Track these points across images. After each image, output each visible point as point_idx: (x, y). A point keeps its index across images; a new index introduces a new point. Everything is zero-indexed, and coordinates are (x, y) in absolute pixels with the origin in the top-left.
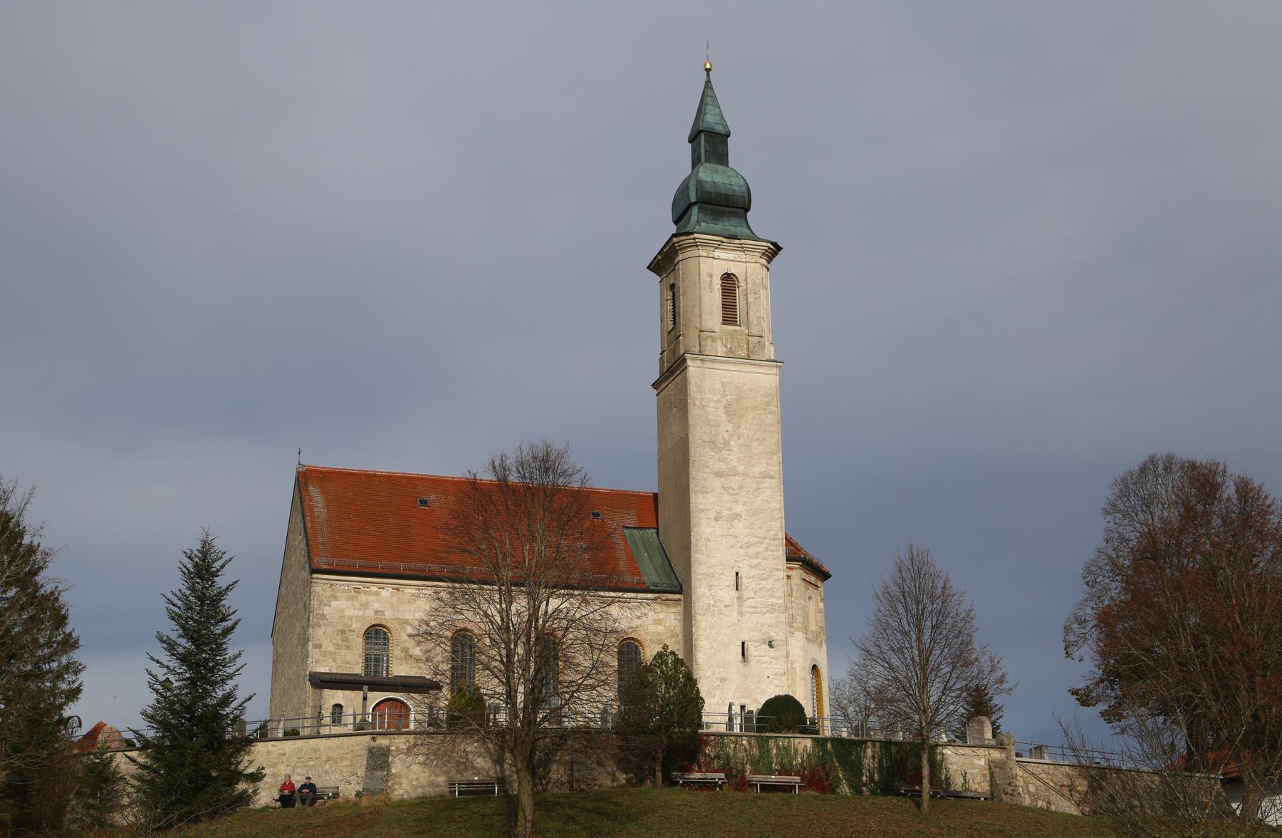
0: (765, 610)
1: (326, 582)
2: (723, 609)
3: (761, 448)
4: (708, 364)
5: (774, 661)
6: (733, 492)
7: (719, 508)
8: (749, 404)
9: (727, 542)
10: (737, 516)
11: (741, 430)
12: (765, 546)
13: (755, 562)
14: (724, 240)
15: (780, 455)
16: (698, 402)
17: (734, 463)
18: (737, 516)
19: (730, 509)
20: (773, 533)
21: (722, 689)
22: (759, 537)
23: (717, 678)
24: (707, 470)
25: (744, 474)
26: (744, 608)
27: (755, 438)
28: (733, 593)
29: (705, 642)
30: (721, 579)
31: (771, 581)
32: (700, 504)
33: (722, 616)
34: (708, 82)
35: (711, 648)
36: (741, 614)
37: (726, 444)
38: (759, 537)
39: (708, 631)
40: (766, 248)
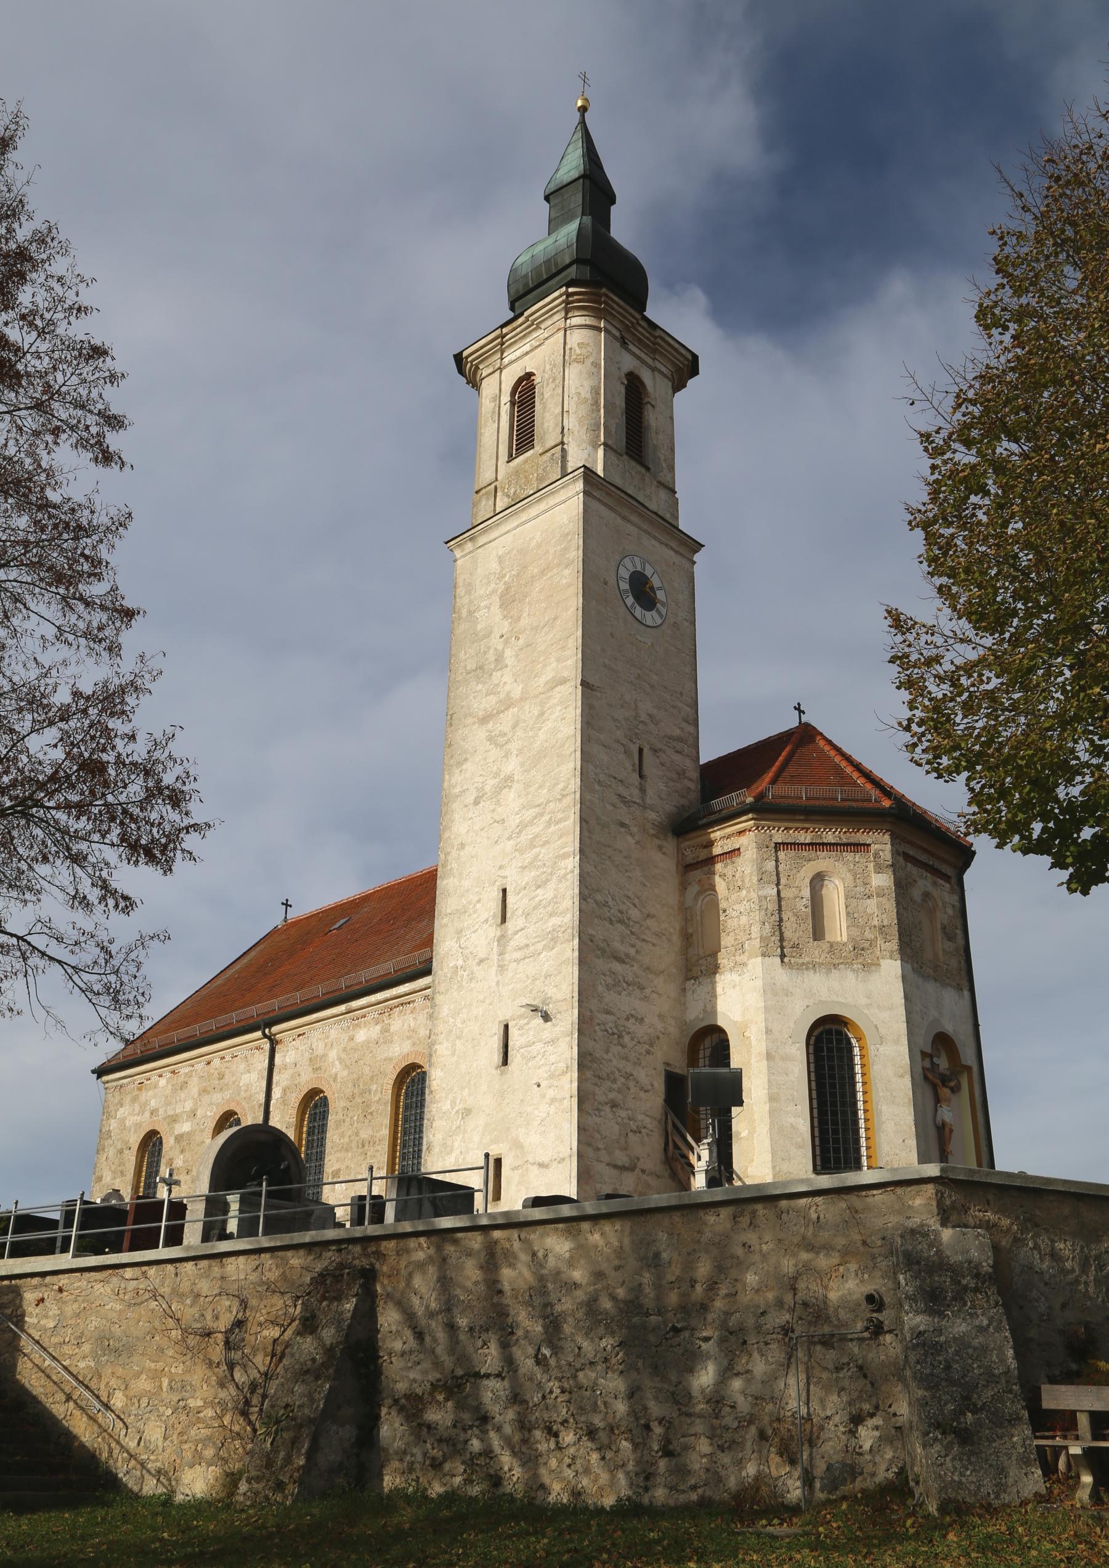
0: (540, 946)
1: (114, 1084)
2: (475, 968)
3: (551, 636)
4: (482, 540)
5: (550, 1048)
6: (501, 740)
7: (481, 779)
8: (536, 570)
9: (488, 838)
10: (508, 781)
11: (525, 621)
12: (546, 817)
13: (529, 856)
14: (505, 330)
15: (580, 633)
16: (464, 613)
17: (507, 688)
18: (508, 781)
19: (496, 775)
20: (561, 786)
21: (465, 1132)
22: (539, 806)
23: (457, 1112)
24: (470, 720)
25: (521, 699)
26: (507, 956)
27: (542, 624)
28: (493, 931)
29: (446, 1044)
30: (475, 912)
31: (552, 885)
32: (455, 786)
33: (472, 985)
34: (583, 122)
35: (453, 1054)
36: (502, 968)
37: (499, 659)
38: (539, 806)
39: (451, 1020)
40: (560, 300)
